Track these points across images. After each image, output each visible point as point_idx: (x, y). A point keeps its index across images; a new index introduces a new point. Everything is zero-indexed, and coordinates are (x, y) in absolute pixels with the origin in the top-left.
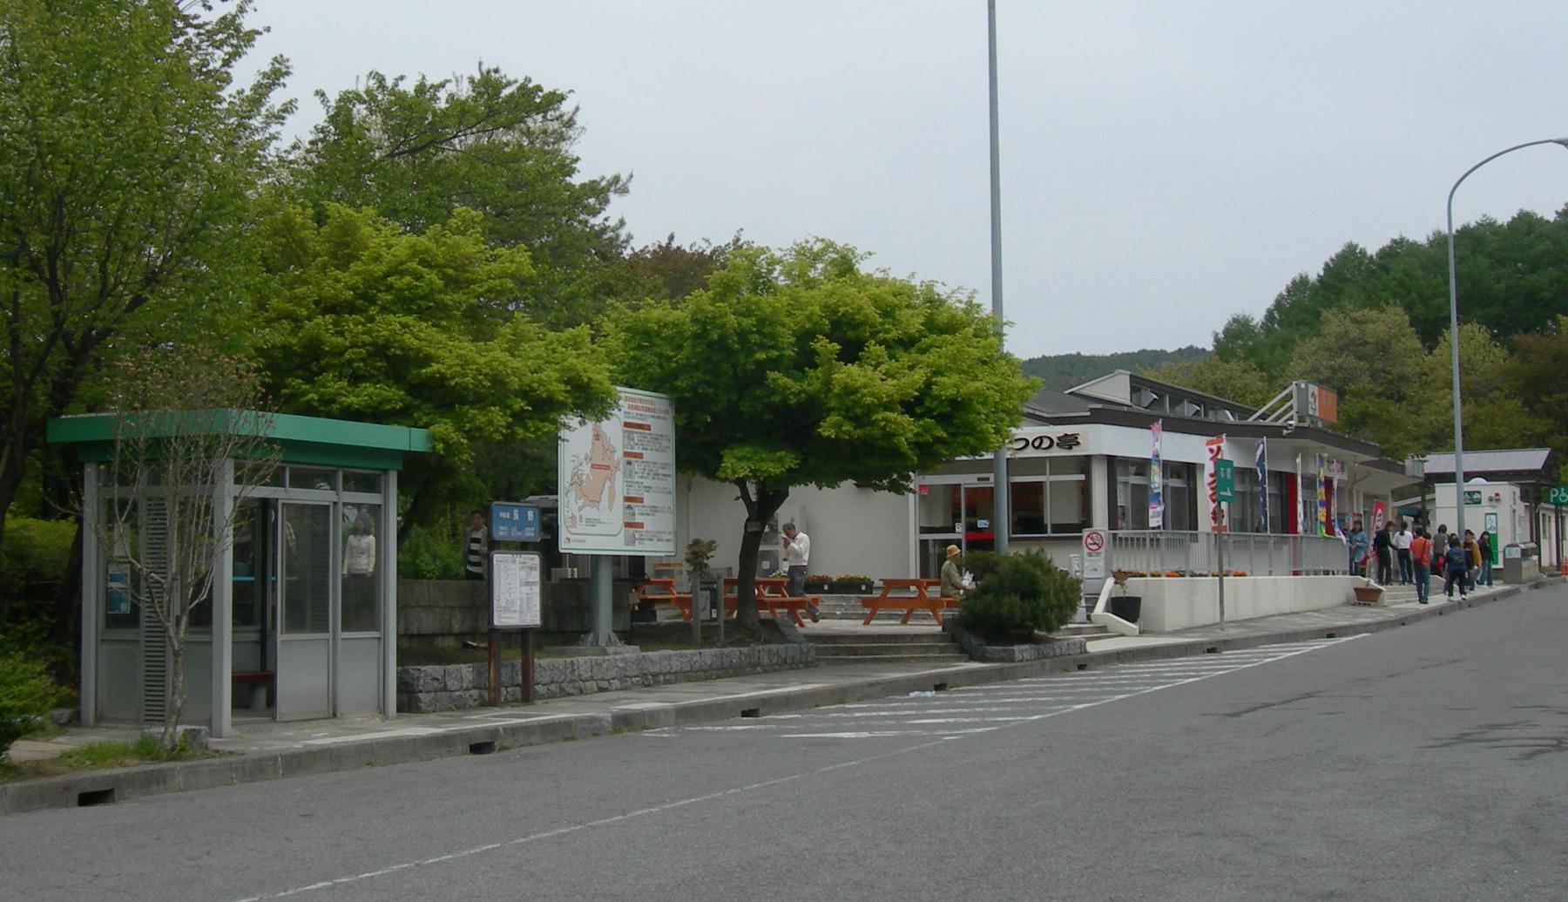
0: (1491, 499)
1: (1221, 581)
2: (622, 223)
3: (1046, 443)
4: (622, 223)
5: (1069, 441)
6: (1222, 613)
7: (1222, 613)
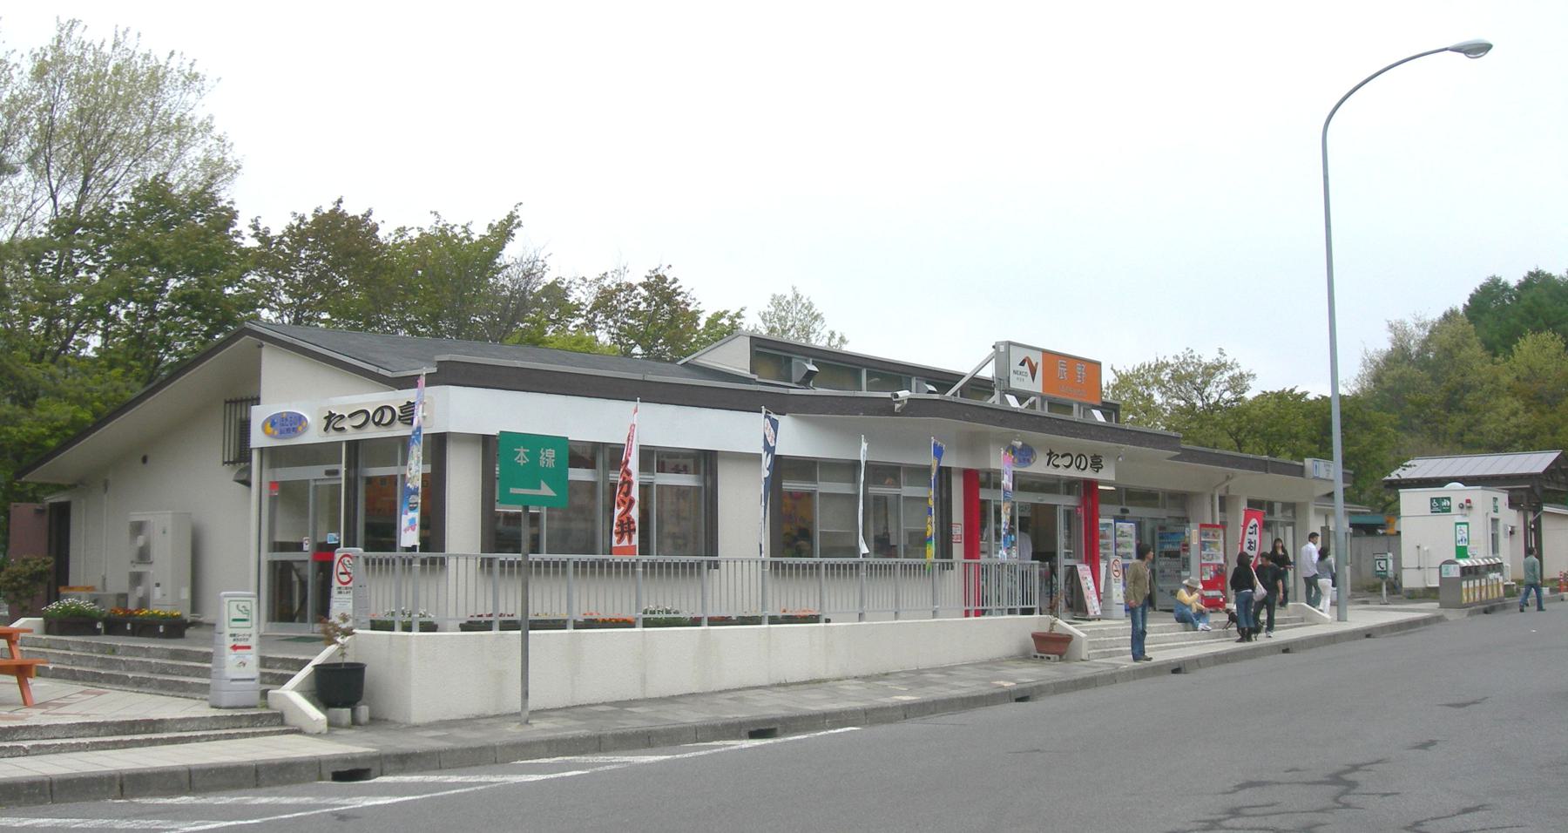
0: (1461, 506)
1: (525, 638)
2: (675, 280)
3: (388, 416)
4: (675, 280)
5: (408, 412)
6: (525, 695)
7: (525, 695)
